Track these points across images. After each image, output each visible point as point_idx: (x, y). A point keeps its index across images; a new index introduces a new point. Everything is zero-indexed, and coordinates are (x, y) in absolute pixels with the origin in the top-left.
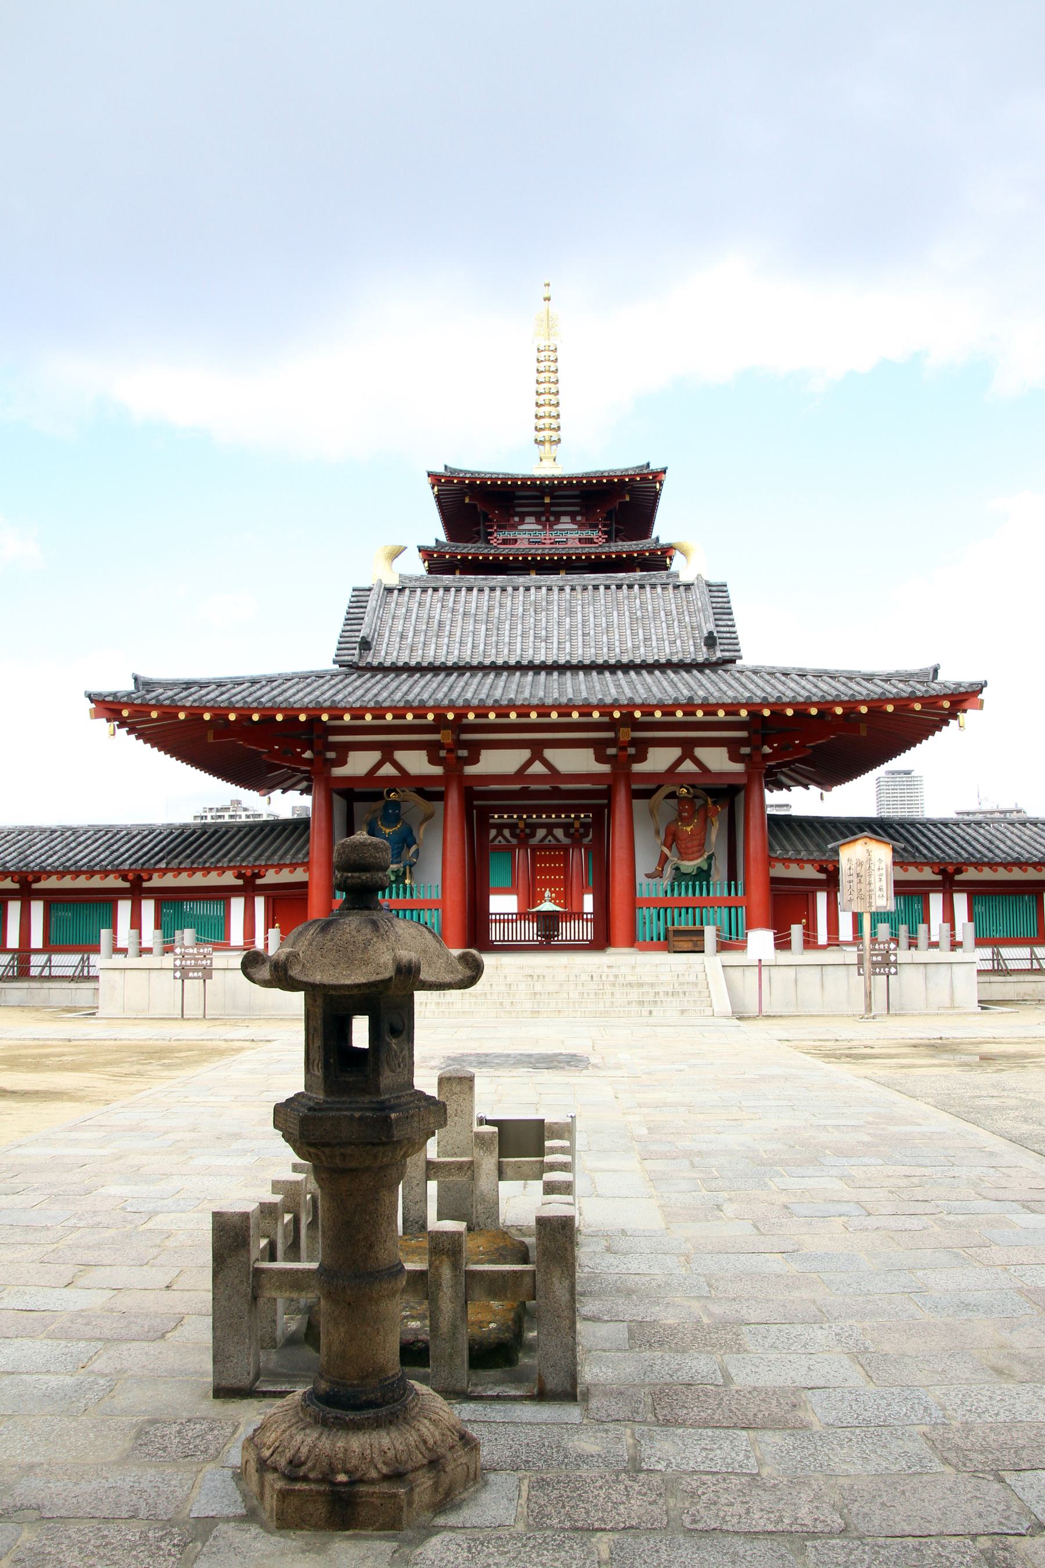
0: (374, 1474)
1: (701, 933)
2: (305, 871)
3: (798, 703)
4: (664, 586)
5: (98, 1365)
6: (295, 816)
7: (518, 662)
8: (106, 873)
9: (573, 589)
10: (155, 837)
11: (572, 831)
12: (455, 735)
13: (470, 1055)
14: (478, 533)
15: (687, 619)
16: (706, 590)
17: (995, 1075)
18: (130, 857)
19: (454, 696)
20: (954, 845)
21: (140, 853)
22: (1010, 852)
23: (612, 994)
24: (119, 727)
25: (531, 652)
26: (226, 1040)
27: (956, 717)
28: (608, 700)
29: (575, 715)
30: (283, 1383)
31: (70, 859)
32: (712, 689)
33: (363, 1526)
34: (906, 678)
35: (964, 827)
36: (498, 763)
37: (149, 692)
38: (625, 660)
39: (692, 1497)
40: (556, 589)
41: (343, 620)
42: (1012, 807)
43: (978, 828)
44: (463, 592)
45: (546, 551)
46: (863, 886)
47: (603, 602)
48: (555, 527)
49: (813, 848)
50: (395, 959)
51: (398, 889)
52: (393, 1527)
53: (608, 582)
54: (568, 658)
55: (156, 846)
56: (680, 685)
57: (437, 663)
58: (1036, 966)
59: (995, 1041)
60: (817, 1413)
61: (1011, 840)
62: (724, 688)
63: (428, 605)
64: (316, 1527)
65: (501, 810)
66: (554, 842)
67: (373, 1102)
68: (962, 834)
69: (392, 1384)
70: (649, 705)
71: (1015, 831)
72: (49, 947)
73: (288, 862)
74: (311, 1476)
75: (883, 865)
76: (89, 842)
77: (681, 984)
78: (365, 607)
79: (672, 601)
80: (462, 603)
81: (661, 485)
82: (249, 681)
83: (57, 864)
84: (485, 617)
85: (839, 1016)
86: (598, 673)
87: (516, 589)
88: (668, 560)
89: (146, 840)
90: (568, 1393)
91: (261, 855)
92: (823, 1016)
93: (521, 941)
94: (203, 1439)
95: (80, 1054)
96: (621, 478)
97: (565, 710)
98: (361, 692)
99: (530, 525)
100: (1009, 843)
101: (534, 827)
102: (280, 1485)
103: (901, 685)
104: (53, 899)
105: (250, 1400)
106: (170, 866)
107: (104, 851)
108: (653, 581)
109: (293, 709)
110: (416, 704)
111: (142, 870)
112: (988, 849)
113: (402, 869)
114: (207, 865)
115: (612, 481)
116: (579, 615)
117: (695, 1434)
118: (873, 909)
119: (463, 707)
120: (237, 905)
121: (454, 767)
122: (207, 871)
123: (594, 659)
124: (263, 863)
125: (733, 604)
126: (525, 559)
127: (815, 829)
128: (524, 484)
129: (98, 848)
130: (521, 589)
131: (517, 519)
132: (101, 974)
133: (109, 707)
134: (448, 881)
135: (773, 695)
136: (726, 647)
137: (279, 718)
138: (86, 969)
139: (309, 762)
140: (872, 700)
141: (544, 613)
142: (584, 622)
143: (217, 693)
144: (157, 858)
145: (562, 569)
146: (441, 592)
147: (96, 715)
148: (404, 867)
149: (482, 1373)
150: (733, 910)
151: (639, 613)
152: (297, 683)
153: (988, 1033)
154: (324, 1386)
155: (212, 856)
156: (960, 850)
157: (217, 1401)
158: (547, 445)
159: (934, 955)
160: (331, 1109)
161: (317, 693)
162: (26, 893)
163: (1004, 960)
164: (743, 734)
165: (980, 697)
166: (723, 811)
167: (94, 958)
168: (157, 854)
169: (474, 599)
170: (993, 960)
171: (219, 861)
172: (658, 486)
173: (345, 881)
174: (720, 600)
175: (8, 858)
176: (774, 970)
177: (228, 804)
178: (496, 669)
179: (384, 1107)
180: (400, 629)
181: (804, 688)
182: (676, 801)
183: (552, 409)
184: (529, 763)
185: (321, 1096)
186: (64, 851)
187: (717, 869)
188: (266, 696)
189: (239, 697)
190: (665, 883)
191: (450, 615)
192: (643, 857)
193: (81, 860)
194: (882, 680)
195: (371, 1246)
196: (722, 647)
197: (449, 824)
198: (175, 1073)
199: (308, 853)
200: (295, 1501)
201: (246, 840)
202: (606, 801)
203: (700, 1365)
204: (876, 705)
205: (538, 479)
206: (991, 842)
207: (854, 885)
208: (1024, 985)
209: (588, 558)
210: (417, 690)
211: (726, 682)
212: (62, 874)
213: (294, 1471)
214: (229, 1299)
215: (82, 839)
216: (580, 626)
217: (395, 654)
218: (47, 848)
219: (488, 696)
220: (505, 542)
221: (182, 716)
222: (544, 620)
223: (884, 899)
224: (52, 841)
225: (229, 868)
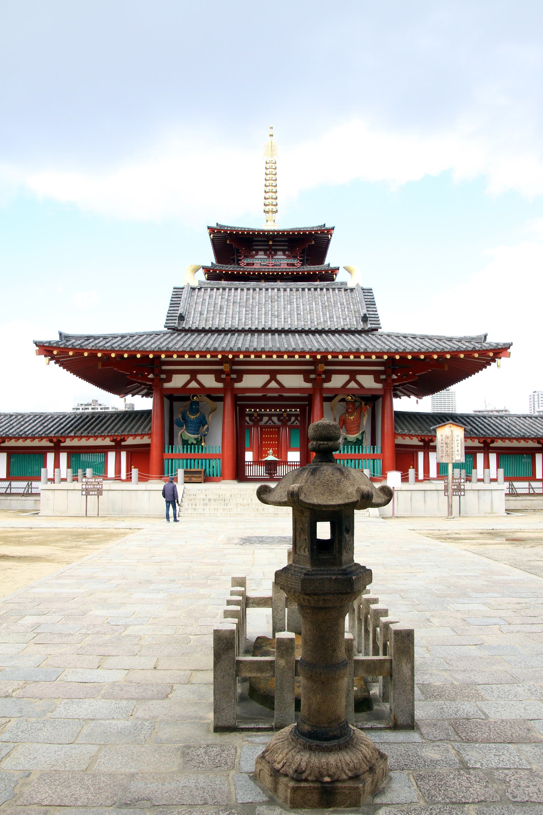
0: (344, 777)
2: (149, 438)
3: (414, 352)
4: (340, 289)
5: (140, 713)
6: (127, 409)
7: (263, 328)
8: (41, 438)
9: (291, 290)
10: (67, 419)
11: (253, 418)
12: (230, 367)
13: (253, 537)
14: (233, 260)
15: (352, 307)
16: (361, 292)
17: (530, 549)
18: (54, 429)
19: (209, 346)
20: (490, 428)
21: (60, 428)
22: (519, 432)
24: (50, 360)
25: (270, 323)
26: (116, 529)
27: (495, 361)
28: (314, 349)
29: (297, 357)
30: (250, 723)
31: (21, 431)
32: (368, 345)
33: (339, 805)
34: (470, 340)
36: (252, 381)
37: (67, 341)
38: (320, 328)
39: (504, 783)
40: (282, 290)
41: (169, 305)
42: (502, 408)
43: (502, 420)
44: (233, 290)
45: (270, 270)
46: (448, 449)
47: (307, 297)
48: (274, 257)
49: (417, 429)
51: (198, 448)
52: (355, 805)
53: (309, 287)
54: (290, 326)
55: (67, 424)
56: (350, 342)
58: (532, 492)
59: (521, 531)
61: (519, 426)
62: (374, 344)
63: (214, 297)
64: (312, 807)
65: (250, 407)
67: (340, 570)
68: (494, 422)
69: (344, 725)
70: (336, 352)
71: (521, 421)
73: (140, 433)
74: (310, 778)
75: (459, 438)
76: (31, 421)
79: (344, 297)
80: (232, 297)
81: (331, 236)
82: (120, 336)
83: (15, 433)
84: (245, 304)
86: (279, 335)
87: (261, 289)
88: (334, 276)
90: (411, 725)
91: (125, 429)
92: (425, 517)
93: (253, 476)
94: (221, 757)
95: (40, 535)
97: (291, 354)
98: (181, 343)
99: (261, 255)
100: (518, 427)
101: (262, 416)
102: (292, 784)
103: (467, 344)
105: (235, 733)
106: (76, 435)
107: (40, 426)
108: (333, 286)
109: (146, 351)
110: (212, 349)
111: (61, 437)
112: (508, 430)
113: (200, 438)
114: (96, 434)
115: (306, 233)
116: (295, 304)
117: (486, 747)
118: (454, 461)
119: (237, 352)
120: (112, 456)
121: (229, 384)
122: (96, 437)
124: (126, 434)
125: (376, 300)
126: (259, 274)
127: (417, 418)
128: (259, 234)
129: (36, 424)
130: (264, 289)
131: (254, 252)
132: (42, 493)
133: (46, 349)
134: (225, 444)
136: (373, 322)
137: (139, 356)
138: (30, 489)
139: (151, 380)
140: (453, 351)
141: (276, 303)
143: (104, 342)
144: (69, 430)
145: (278, 279)
146: (221, 290)
147: (39, 353)
148: (201, 436)
149: (361, 714)
151: (326, 303)
152: (146, 338)
153: (516, 527)
154: (306, 728)
155: (99, 429)
156: (493, 431)
157: (216, 734)
158: (270, 213)
160: (318, 574)
161: (158, 343)
163: (515, 489)
164: (382, 368)
165: (509, 350)
167: (35, 484)
168: (69, 428)
169: (239, 294)
171: (102, 432)
172: (329, 236)
173: (319, 446)
174: (369, 297)
176: (399, 492)
177: (90, 402)
178: (251, 331)
179: (345, 573)
180: (200, 310)
181: (416, 344)
182: (345, 403)
183: (273, 194)
184: (269, 382)
185: (308, 567)
186: (18, 426)
187: (366, 440)
188: (131, 344)
189: (116, 345)
191: (226, 303)
193: (28, 431)
195: (335, 650)
196: (371, 322)
197: (226, 414)
198: (97, 546)
199: (150, 429)
200: (301, 793)
202: (307, 403)
203: (467, 708)
204: (455, 354)
205: (266, 231)
206: (509, 427)
209: (292, 274)
210: (211, 342)
212: (17, 439)
213: (298, 775)
214: (223, 678)
215: (27, 420)
216: (295, 310)
217: (197, 323)
218: (8, 424)
219: (234, 346)
220: (248, 264)
221: (86, 354)
222: (276, 306)
223: (459, 456)
224: (11, 421)
225: (108, 436)
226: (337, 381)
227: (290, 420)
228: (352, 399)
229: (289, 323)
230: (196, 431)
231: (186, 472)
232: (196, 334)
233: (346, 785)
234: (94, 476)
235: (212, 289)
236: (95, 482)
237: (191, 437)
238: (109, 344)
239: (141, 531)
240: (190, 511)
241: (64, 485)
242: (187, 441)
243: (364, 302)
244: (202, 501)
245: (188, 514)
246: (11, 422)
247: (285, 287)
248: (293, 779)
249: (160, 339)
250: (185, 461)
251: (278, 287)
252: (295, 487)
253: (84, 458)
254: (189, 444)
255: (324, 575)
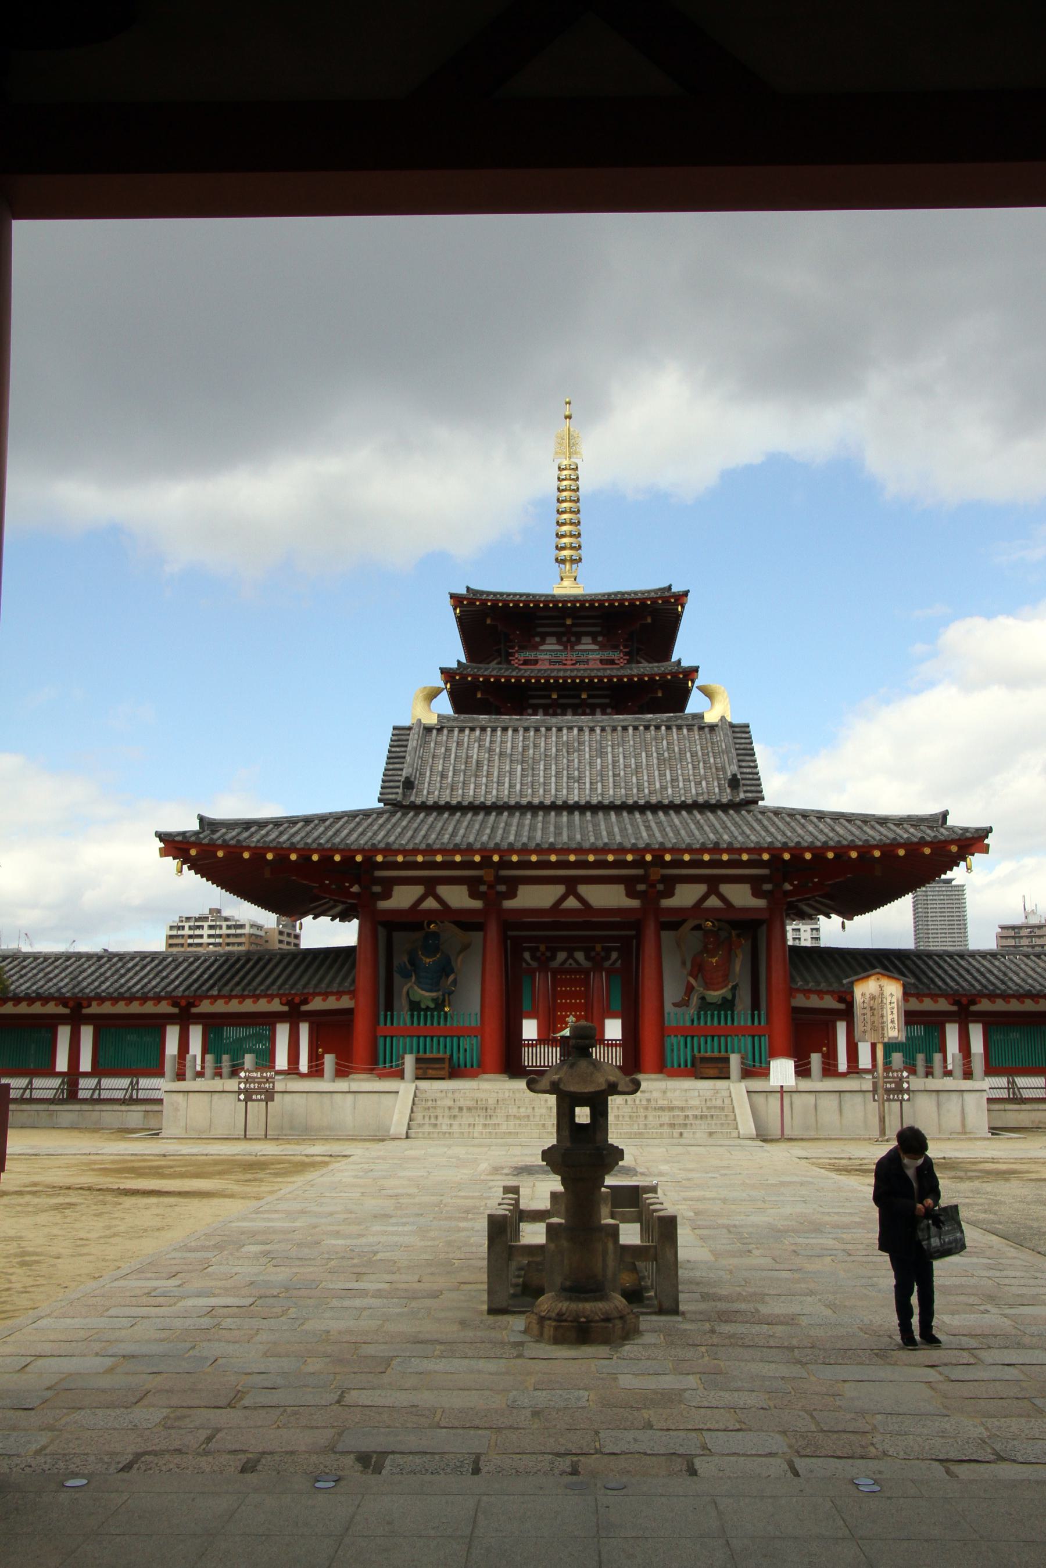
0: (597, 1318)
1: (727, 1060)
2: (351, 999)
3: (817, 848)
4: (690, 728)
7: (553, 803)
8: (158, 999)
9: (603, 730)
11: (593, 954)
12: (494, 874)
15: (712, 760)
18: (181, 983)
20: (968, 977)
21: (190, 980)
22: (1022, 984)
23: (646, 1117)
24: (183, 863)
25: (565, 792)
26: (307, 1156)
27: (965, 860)
28: (641, 845)
35: (979, 958)
37: (214, 832)
38: (654, 800)
40: (587, 730)
45: (568, 674)
46: (876, 1018)
47: (631, 743)
48: (577, 647)
50: (607, 1081)
51: (439, 1017)
53: (636, 723)
57: (477, 803)
59: (993, 1160)
60: (804, 1321)
66: (574, 965)
72: (98, 1070)
73: (335, 990)
75: (894, 1000)
76: (138, 968)
77: (709, 1108)
78: (406, 746)
80: (498, 744)
81: (683, 607)
82: (303, 820)
84: (520, 757)
85: (856, 1139)
89: (193, 968)
90: (675, 1311)
92: (842, 1139)
96: (643, 601)
99: (551, 645)
104: (103, 1025)
107: (154, 978)
108: (679, 722)
109: (350, 850)
114: (258, 992)
116: (610, 756)
118: (886, 1040)
120: (282, 1033)
123: (624, 799)
124: (311, 991)
130: (554, 729)
131: (538, 639)
132: (166, 1098)
135: (793, 839)
136: (749, 788)
140: (885, 845)
141: (576, 754)
142: (614, 762)
144: (207, 985)
146: (478, 732)
148: (444, 995)
150: (756, 1038)
151: (666, 754)
153: (988, 1154)
154: (568, 1283)
156: (974, 982)
159: (949, 1083)
162: (76, 1019)
163: (1019, 1089)
164: (765, 871)
165: (986, 841)
166: (746, 944)
169: (510, 739)
170: (1008, 1089)
171: (268, 988)
174: (743, 741)
175: (62, 984)
180: (440, 769)
181: (822, 831)
185: (569, 1145)
190: (692, 1011)
191: (487, 755)
192: (671, 987)
194: (895, 824)
196: (745, 788)
199: (353, 981)
201: (291, 968)
202: (634, 933)
204: (889, 849)
205: (560, 601)
207: (868, 1017)
208: (1039, 1114)
211: (748, 824)
212: (115, 1000)
213: (560, 1317)
215: (130, 965)
216: (610, 767)
217: (436, 793)
219: (529, 838)
220: (526, 662)
222: (576, 761)
223: (894, 1030)
224: (100, 967)
226: (686, 896)
227: (608, 958)
228: (714, 926)
229: (599, 791)
230: (434, 986)
231: (418, 1060)
232: (435, 814)
233: (599, 1324)
234: (258, 1067)
235: (462, 730)
236: (262, 1077)
237: (425, 996)
238: (285, 837)
239: (351, 1159)
240: (427, 1129)
241: (200, 1084)
242: (419, 1003)
243: (734, 751)
244: (447, 1111)
245: (423, 1133)
246: (103, 970)
247: (591, 724)
248: (555, 1320)
249: (371, 824)
250: (415, 1039)
251: (579, 724)
252: (556, 1077)
253: (231, 1033)
254: (423, 1010)
255: (582, 1154)
